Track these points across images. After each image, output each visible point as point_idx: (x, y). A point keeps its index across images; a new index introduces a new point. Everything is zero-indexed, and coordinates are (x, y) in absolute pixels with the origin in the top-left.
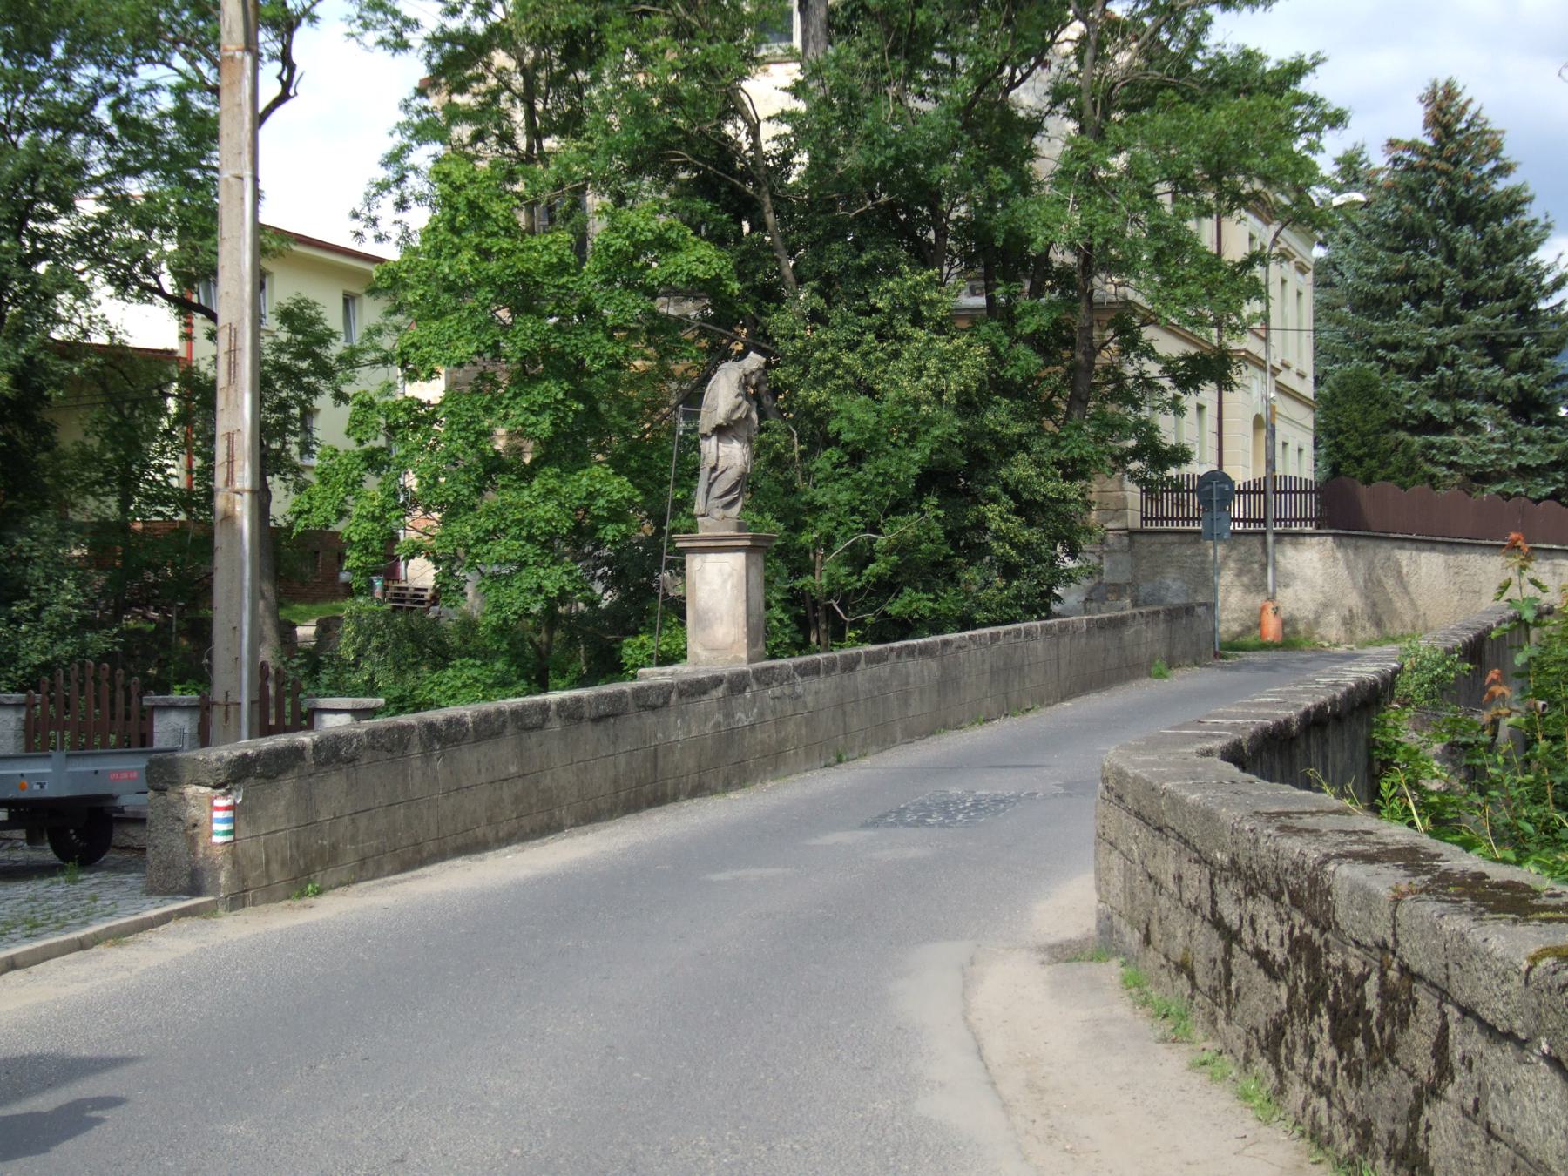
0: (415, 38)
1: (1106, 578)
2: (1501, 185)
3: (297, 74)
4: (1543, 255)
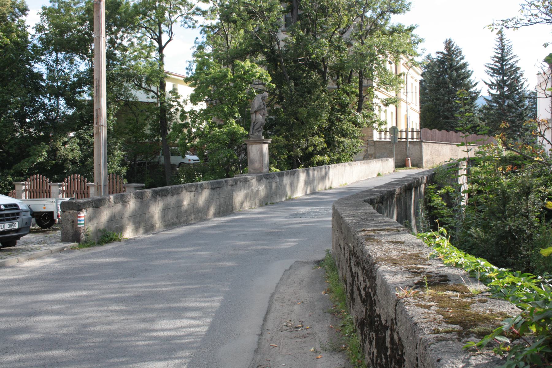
0: (197, 25)
1: (369, 153)
2: (462, 62)
3: (173, 34)
4: (472, 78)
